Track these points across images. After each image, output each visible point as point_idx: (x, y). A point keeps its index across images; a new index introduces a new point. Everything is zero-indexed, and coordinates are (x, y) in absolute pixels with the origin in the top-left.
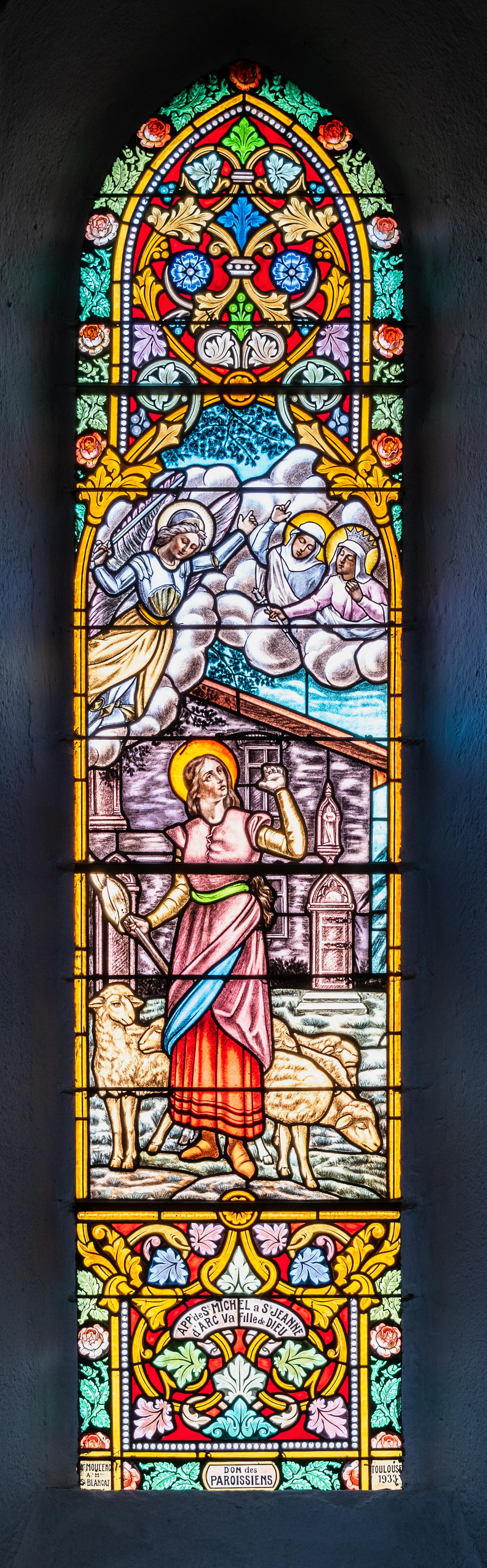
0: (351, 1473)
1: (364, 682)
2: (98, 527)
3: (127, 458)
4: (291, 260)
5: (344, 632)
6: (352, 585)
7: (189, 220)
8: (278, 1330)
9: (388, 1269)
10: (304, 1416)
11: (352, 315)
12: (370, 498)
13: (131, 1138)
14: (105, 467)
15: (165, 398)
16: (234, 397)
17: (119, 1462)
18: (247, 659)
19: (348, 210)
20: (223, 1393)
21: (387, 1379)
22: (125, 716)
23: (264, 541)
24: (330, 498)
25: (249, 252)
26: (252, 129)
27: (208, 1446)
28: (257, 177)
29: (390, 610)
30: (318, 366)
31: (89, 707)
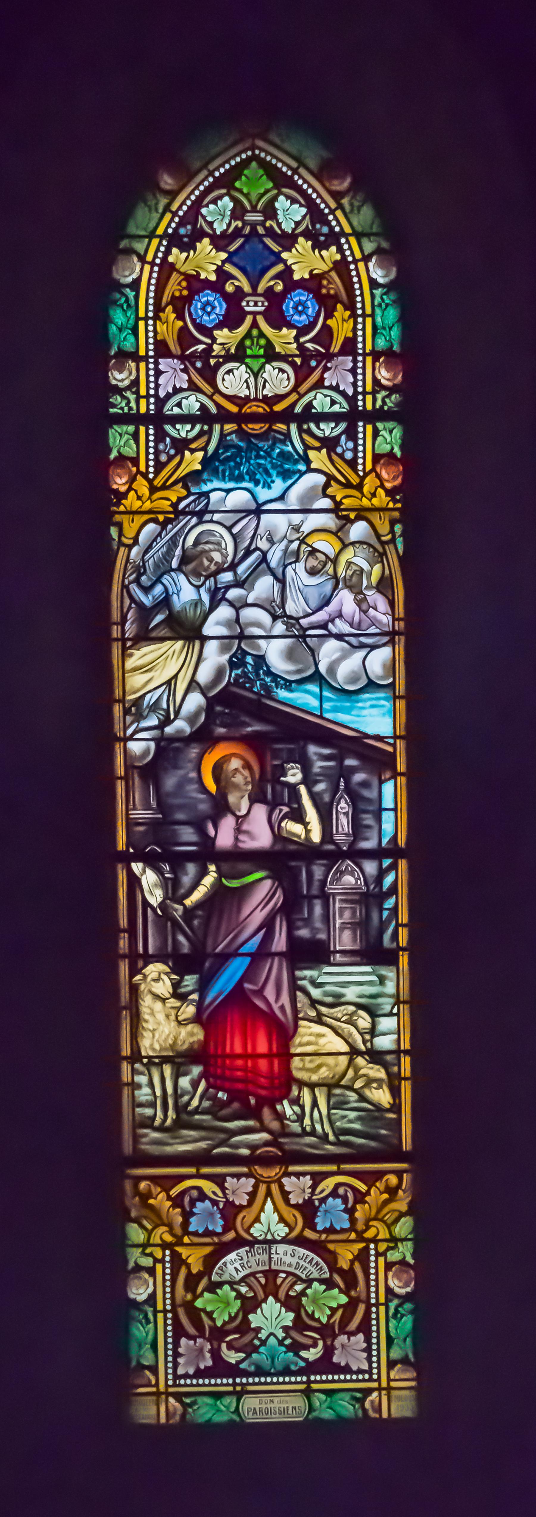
0: (372, 1402)
1: (371, 685)
2: (130, 547)
3: (155, 483)
4: (300, 296)
5: (353, 640)
6: (360, 597)
7: (207, 259)
8: (305, 1272)
9: (402, 1215)
10: (329, 1351)
11: (357, 348)
12: (375, 518)
13: (170, 1102)
14: (136, 491)
15: (188, 427)
16: (250, 426)
17: (163, 1397)
18: (268, 667)
19: (350, 248)
20: (258, 1330)
21: (403, 1316)
22: (159, 718)
23: (281, 558)
24: (339, 517)
25: (261, 289)
26: (261, 172)
27: (244, 1380)
28: (267, 218)
29: (394, 620)
30: (326, 396)
31: (127, 712)
